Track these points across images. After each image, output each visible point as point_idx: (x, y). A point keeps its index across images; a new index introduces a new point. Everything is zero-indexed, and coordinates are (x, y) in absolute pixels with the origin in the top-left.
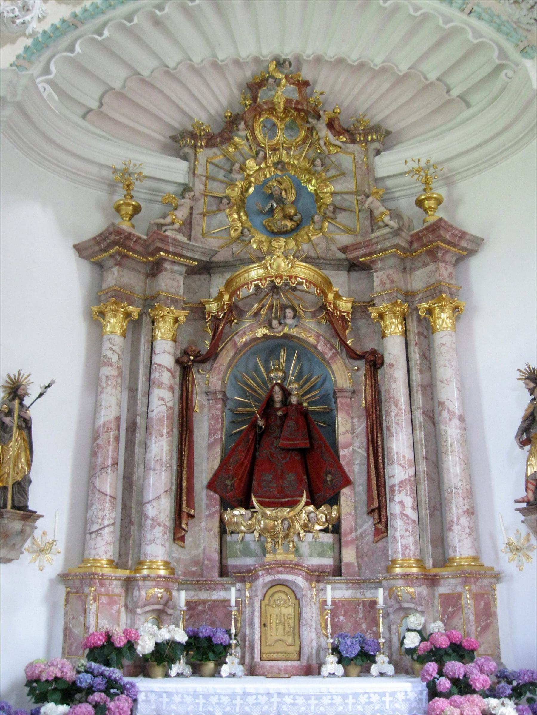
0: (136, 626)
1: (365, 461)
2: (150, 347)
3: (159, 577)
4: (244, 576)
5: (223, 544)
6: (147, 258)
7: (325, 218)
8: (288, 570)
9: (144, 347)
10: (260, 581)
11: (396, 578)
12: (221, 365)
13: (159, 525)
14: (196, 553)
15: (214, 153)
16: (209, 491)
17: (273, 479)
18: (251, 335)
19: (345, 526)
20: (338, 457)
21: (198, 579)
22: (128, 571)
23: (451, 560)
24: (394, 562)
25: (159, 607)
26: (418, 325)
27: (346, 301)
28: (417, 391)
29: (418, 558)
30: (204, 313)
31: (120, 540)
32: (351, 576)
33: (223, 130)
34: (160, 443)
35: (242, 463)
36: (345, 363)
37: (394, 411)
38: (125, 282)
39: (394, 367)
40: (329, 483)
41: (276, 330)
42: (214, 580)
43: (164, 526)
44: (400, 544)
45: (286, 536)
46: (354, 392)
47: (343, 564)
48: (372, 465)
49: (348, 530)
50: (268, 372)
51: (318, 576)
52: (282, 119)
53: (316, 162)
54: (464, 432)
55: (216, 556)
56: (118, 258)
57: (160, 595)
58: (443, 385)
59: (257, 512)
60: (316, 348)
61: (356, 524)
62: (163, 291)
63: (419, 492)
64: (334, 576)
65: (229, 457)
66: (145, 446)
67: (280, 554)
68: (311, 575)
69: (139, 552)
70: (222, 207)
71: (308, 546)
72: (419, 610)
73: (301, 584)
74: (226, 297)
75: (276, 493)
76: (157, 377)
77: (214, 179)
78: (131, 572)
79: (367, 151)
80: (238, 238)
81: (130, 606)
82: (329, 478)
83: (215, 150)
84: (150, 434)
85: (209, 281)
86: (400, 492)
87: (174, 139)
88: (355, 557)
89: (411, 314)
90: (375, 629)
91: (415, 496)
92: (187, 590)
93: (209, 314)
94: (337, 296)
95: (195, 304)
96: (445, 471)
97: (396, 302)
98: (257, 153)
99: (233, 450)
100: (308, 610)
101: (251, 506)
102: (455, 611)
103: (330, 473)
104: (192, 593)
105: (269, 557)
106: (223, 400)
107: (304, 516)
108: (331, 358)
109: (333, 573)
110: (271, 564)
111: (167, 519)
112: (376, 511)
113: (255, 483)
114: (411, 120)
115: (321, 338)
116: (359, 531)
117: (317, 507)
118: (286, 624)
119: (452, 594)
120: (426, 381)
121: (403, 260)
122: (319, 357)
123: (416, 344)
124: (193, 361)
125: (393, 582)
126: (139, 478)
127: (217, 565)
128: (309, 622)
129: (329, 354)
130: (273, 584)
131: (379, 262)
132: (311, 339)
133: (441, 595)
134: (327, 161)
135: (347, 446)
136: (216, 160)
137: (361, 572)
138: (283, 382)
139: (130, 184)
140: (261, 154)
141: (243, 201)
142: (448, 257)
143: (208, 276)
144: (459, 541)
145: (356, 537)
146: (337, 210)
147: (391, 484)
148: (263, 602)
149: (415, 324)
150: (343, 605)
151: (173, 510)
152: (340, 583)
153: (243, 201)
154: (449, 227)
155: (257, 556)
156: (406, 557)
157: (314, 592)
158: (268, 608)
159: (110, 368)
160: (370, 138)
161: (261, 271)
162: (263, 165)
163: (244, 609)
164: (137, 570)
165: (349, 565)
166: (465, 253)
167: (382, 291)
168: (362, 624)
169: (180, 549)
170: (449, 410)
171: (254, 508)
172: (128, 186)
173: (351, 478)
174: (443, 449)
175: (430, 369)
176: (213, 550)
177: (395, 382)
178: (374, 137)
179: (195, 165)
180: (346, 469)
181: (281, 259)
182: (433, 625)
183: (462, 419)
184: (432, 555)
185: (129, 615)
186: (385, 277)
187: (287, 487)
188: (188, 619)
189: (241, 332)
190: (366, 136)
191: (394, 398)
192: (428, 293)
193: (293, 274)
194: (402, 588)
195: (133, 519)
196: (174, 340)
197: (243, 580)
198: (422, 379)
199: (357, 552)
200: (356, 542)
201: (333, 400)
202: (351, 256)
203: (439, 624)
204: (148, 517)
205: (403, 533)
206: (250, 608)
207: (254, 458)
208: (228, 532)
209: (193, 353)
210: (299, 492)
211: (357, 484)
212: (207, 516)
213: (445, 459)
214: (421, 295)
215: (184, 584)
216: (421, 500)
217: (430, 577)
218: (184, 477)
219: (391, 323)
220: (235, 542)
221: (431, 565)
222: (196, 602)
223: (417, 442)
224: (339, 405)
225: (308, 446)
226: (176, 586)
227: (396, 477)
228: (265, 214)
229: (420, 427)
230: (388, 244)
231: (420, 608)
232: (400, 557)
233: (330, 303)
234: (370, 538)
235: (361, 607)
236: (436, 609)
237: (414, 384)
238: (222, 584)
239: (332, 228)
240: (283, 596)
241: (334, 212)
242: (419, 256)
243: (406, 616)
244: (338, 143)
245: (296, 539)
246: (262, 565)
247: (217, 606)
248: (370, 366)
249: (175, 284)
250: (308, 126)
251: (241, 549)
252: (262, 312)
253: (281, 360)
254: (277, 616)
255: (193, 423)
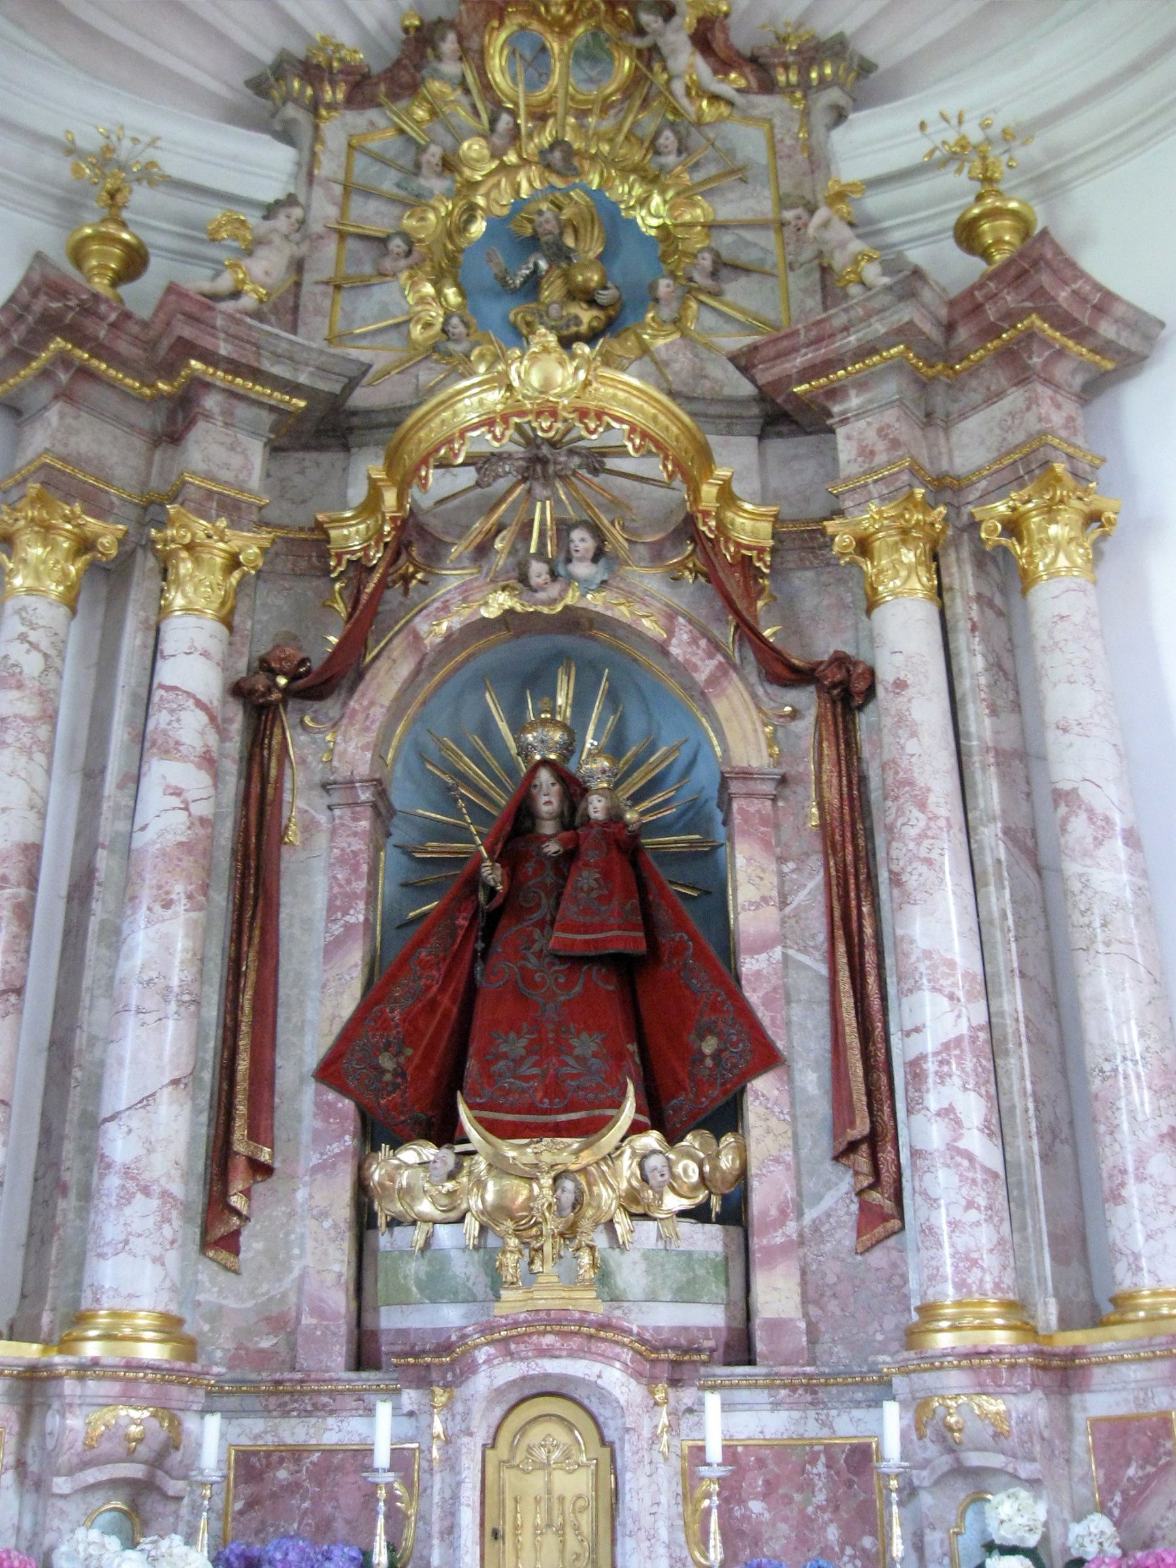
0: (49, 1539)
1: (823, 992)
2: (151, 642)
3: (132, 1366)
4: (428, 1366)
5: (367, 1260)
6: (152, 386)
7: (689, 289)
8: (575, 1343)
9: (132, 640)
10: (481, 1383)
11: (941, 1368)
12: (372, 703)
13: (146, 1191)
14: (276, 1291)
15: (372, 123)
16: (323, 1088)
17: (529, 1050)
18: (467, 612)
19: (761, 1199)
20: (738, 979)
21: (278, 1376)
22: (35, 1346)
23: (1122, 1303)
24: (929, 1311)
25: (135, 1471)
26: (976, 577)
27: (755, 516)
28: (984, 768)
29: (1011, 1296)
30: (325, 555)
31: (28, 1245)
32: (786, 1363)
33: (398, 63)
34: (164, 928)
35: (433, 1004)
36: (754, 696)
37: (913, 823)
38: (83, 448)
39: (910, 692)
40: (709, 1062)
41: (541, 595)
42: (331, 1380)
43: (165, 1194)
44: (947, 1250)
45: (569, 1233)
46: (783, 781)
47: (757, 1322)
48: (847, 1002)
49: (774, 1212)
50: (518, 726)
51: (675, 1364)
52: (564, 30)
53: (661, 141)
54: (1142, 882)
55: (340, 1301)
56: (63, 377)
57: (134, 1430)
58: (1066, 739)
59: (474, 1153)
60: (666, 653)
61: (799, 1193)
62: (194, 473)
63: (1003, 1080)
64: (728, 1363)
65: (392, 978)
66: (114, 937)
67: (548, 1287)
68: (653, 1362)
69: (78, 1285)
70: (388, 264)
71: (642, 1266)
72: (1023, 1474)
73: (617, 1392)
74: (390, 498)
75: (539, 1095)
76: (163, 725)
77: (368, 193)
78: (44, 1351)
79: (806, 113)
80: (435, 348)
81: (33, 1467)
82: (709, 1046)
83: (372, 114)
84: (133, 898)
85: (345, 470)
86: (942, 1078)
87: (259, 86)
88: (797, 1299)
89: (955, 543)
90: (867, 1542)
91: (993, 1091)
92: (229, 1415)
93: (339, 556)
94: (727, 496)
95: (301, 529)
96: (1087, 1006)
97: (911, 495)
98: (493, 121)
99: (403, 962)
100: (644, 1481)
101: (457, 1136)
102: (1149, 1478)
103: (710, 1031)
104: (256, 1425)
105: (512, 1302)
106: (374, 806)
107: (627, 1165)
108: (713, 680)
109: (726, 1352)
110: (516, 1324)
111: (176, 1174)
112: (864, 1148)
113: (472, 1065)
114: (932, 32)
115: (681, 620)
116: (810, 1215)
117: (672, 1137)
118: (569, 1531)
119: (1138, 1418)
120: (1009, 741)
121: (924, 385)
122: (673, 684)
123: (974, 629)
124: (285, 691)
125: (930, 1379)
126: (92, 1040)
127: (342, 1328)
128: (646, 1521)
129: (705, 669)
130: (527, 1392)
131: (853, 392)
132: (646, 622)
133: (1096, 1423)
134: (695, 138)
135: (763, 946)
136: (374, 144)
137: (819, 1348)
138: (566, 758)
139: (118, 190)
140: (505, 120)
141: (453, 260)
142: (1062, 371)
143: (341, 455)
144: (1149, 1237)
145: (801, 1235)
146: (724, 272)
147: (911, 1056)
148: (489, 1453)
149: (969, 569)
150: (761, 1463)
151: (202, 1151)
152: (749, 1387)
153: (453, 260)
154: (1068, 269)
155: (471, 1299)
156: (970, 1293)
157: (664, 1420)
158: (508, 1475)
159: (14, 694)
160: (814, 75)
161: (494, 398)
162: (511, 158)
163: (426, 1476)
164: (66, 1345)
165: (777, 1326)
166: (1109, 365)
167: (865, 473)
168: (826, 1524)
169: (224, 1277)
170: (1091, 814)
171: (467, 1141)
172: (112, 195)
173: (780, 1045)
174: (1079, 939)
175: (1017, 706)
176: (330, 1279)
177: (914, 734)
178: (828, 71)
179: (313, 154)
180: (764, 1015)
181: (554, 356)
182: (1077, 1529)
183: (1132, 839)
184: (1055, 1288)
185: (30, 1498)
186: (871, 436)
187: (574, 1077)
188: (241, 1513)
189: (437, 604)
190: (804, 72)
191: (911, 783)
192: (1007, 475)
193: (592, 405)
194: (963, 1400)
195: (66, 1176)
196: (227, 621)
197: (423, 1382)
198: (996, 732)
199: (804, 1283)
200: (801, 1252)
201: (719, 816)
202: (765, 376)
203: (1099, 1524)
204: (109, 1166)
205: (958, 1213)
206: (446, 1474)
207: (471, 991)
208: (381, 1221)
209: (286, 666)
210: (615, 1092)
211: (798, 1065)
212: (315, 1170)
213: (1086, 968)
214: (983, 484)
215: (229, 1393)
216: (1013, 1108)
217: (1056, 1362)
218: (244, 1042)
219: (896, 564)
220: (402, 1252)
221: (1054, 1320)
222: (269, 1454)
223: (991, 922)
224: (737, 819)
225: (642, 949)
226: (199, 1398)
227: (928, 1031)
228: (514, 292)
229: (1000, 878)
230: (879, 328)
231: (1026, 1470)
232: (950, 1293)
233: (706, 514)
234: (846, 1237)
235: (820, 1468)
236: (1078, 1471)
237: (973, 744)
238: (357, 1394)
239: (709, 319)
240: (559, 1434)
241: (714, 274)
242: (973, 372)
243: (978, 1498)
244: (725, 89)
245: (601, 1240)
246: (487, 1329)
247: (340, 1468)
248: (834, 703)
249: (236, 461)
250: (639, 43)
251: (423, 1276)
252: (498, 545)
253: (560, 701)
254: (537, 1501)
255: (278, 873)
